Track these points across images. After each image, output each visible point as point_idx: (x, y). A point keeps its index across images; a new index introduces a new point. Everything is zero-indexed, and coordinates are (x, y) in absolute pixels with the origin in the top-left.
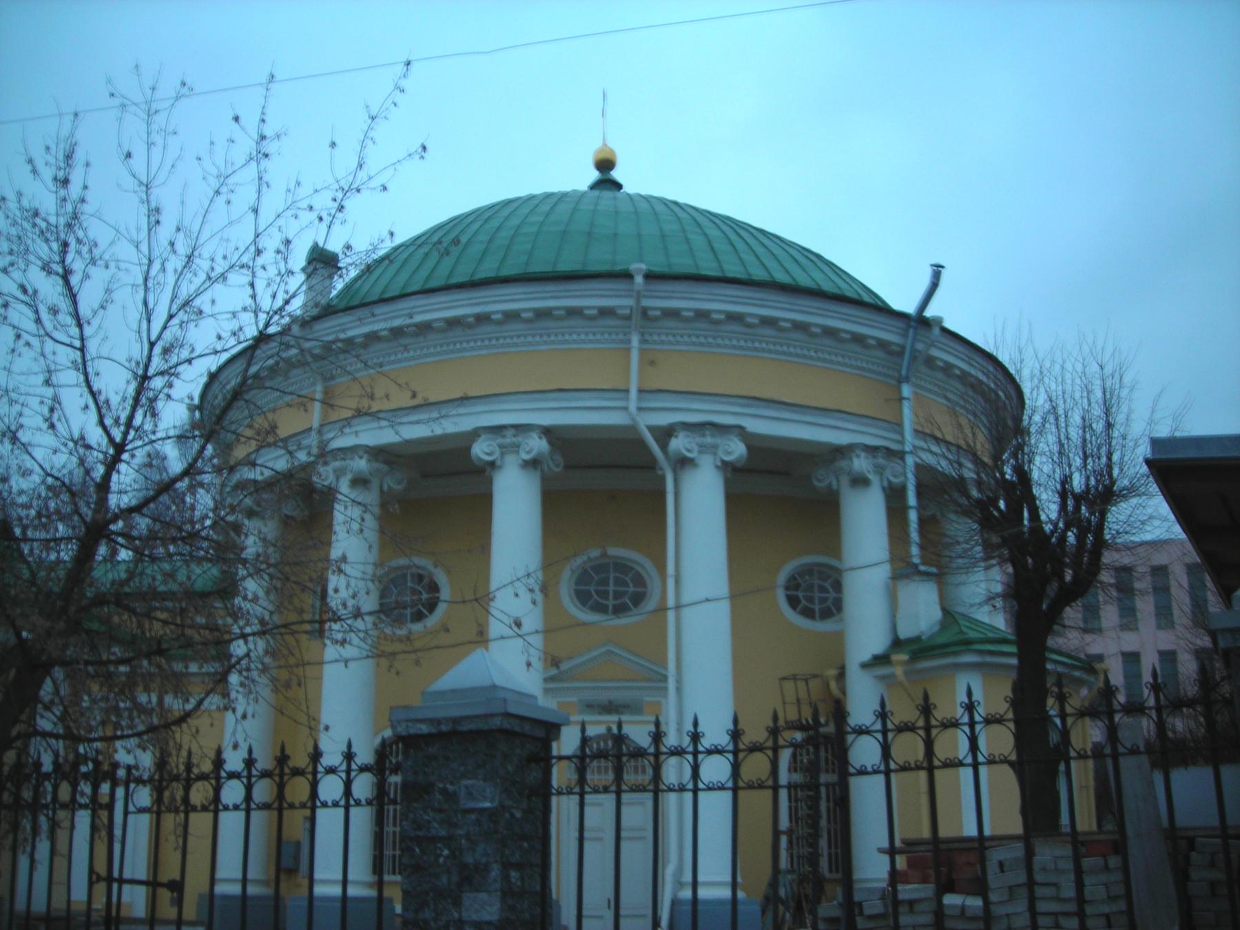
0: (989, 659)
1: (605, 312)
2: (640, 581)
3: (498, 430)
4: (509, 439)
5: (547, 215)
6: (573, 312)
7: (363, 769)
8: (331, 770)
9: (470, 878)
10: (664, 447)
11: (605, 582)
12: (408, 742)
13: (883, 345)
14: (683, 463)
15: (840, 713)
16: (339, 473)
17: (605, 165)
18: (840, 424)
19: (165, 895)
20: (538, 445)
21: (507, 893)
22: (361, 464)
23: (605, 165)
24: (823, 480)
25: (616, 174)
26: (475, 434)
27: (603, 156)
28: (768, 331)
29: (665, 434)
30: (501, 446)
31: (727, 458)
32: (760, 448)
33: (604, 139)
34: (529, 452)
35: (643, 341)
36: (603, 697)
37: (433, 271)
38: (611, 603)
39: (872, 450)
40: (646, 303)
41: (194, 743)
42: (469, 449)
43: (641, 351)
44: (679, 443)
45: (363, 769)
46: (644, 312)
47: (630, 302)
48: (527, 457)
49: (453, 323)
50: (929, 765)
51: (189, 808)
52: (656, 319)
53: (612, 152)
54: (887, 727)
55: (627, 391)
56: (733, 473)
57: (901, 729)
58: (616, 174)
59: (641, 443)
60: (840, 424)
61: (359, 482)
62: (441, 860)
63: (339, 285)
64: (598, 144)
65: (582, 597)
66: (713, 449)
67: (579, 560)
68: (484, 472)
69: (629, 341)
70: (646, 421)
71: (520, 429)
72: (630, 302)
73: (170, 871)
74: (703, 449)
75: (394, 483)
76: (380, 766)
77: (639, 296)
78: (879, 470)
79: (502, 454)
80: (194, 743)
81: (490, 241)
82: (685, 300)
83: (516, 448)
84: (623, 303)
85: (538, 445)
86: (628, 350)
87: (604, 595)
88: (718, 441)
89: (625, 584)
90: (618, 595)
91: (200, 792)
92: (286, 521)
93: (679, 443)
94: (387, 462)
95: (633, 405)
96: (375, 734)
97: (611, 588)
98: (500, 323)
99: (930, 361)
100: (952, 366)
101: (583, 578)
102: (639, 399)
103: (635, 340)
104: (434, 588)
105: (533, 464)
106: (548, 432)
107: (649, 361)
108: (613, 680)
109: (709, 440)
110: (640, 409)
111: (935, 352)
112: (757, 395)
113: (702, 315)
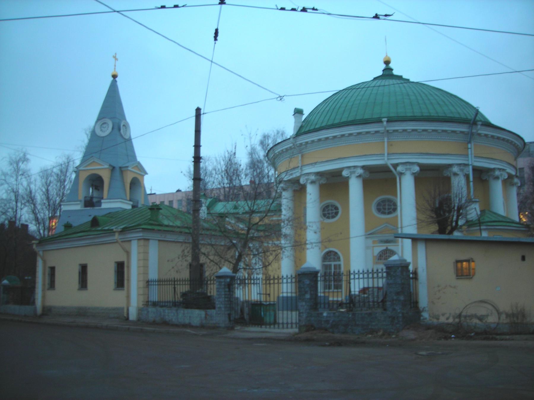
0: (489, 227)
1: (377, 132)
3: (349, 167)
4: (352, 170)
5: (363, 96)
6: (368, 133)
9: (306, 293)
10: (395, 169)
11: (385, 205)
12: (299, 275)
13: (462, 132)
14: (401, 174)
15: (350, 272)
17: (387, 62)
18: (449, 158)
19: (268, 296)
20: (360, 171)
21: (311, 294)
22: (313, 178)
23: (387, 62)
24: (446, 173)
27: (386, 60)
28: (425, 133)
29: (395, 166)
32: (424, 168)
33: (387, 54)
35: (388, 139)
36: (385, 238)
38: (387, 211)
39: (459, 165)
40: (387, 129)
41: (272, 271)
43: (388, 142)
44: (399, 169)
46: (388, 131)
47: (383, 129)
48: (358, 175)
49: (335, 137)
51: (270, 284)
52: (391, 133)
53: (389, 58)
54: (330, 281)
55: (384, 154)
60: (449, 158)
63: (304, 117)
64: (384, 56)
65: (379, 210)
66: (410, 169)
69: (384, 139)
71: (355, 167)
72: (383, 129)
73: (268, 292)
74: (407, 169)
75: (323, 181)
76: (295, 277)
77: (385, 127)
78: (462, 170)
79: (351, 174)
80: (272, 271)
81: (346, 106)
82: (399, 126)
83: (354, 172)
84: (381, 129)
85: (360, 171)
86: (384, 142)
87: (385, 209)
88: (411, 167)
90: (389, 209)
91: (272, 282)
92: (295, 191)
94: (321, 176)
95: (386, 158)
96: (322, 252)
97: (387, 207)
98: (348, 136)
99: (479, 135)
100: (488, 135)
102: (388, 156)
103: (386, 140)
105: (360, 176)
106: (363, 167)
107: (390, 145)
109: (408, 167)
110: (388, 159)
111: (479, 132)
113: (404, 131)
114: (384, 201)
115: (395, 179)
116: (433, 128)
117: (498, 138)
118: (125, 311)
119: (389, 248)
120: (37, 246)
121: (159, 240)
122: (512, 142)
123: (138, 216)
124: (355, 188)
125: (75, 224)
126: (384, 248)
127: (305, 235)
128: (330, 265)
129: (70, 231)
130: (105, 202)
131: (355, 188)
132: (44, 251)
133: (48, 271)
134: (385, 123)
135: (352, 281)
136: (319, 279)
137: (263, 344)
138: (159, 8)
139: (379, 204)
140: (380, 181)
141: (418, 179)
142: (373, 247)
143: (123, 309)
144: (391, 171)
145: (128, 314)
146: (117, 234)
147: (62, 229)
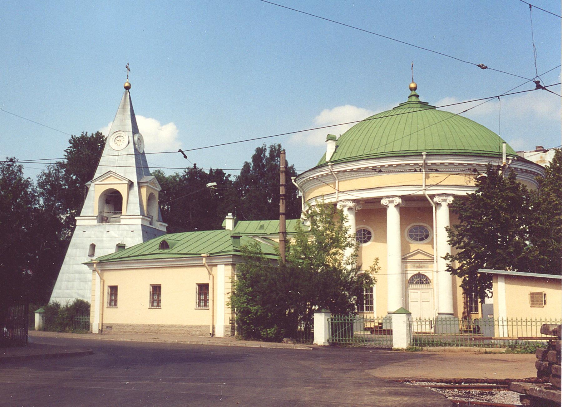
2: (427, 231)
3: (388, 197)
4: (391, 199)
14: (438, 205)
16: (344, 206)
22: (351, 204)
25: (417, 92)
29: (432, 197)
42: (380, 202)
44: (436, 199)
47: (423, 162)
50: (421, 325)
58: (417, 92)
61: (350, 209)
66: (445, 200)
67: (409, 227)
68: (383, 210)
70: (427, 193)
71: (393, 196)
75: (358, 208)
85: (398, 201)
93: (436, 199)
94: (357, 202)
101: (411, 231)
104: (369, 233)
106: (402, 197)
108: (369, 158)
109: (444, 198)
112: (457, 184)
114: (416, 228)
115: (432, 207)
116: (478, 163)
117: (527, 171)
119: (421, 272)
120: (97, 265)
121: (225, 264)
124: (393, 216)
125: (128, 245)
126: (417, 272)
129: (123, 253)
130: (79, 219)
131: (393, 216)
132: (101, 270)
133: (107, 290)
134: (424, 157)
140: (417, 211)
141: (454, 210)
144: (427, 200)
145: (213, 331)
146: (204, 259)
147: (113, 250)
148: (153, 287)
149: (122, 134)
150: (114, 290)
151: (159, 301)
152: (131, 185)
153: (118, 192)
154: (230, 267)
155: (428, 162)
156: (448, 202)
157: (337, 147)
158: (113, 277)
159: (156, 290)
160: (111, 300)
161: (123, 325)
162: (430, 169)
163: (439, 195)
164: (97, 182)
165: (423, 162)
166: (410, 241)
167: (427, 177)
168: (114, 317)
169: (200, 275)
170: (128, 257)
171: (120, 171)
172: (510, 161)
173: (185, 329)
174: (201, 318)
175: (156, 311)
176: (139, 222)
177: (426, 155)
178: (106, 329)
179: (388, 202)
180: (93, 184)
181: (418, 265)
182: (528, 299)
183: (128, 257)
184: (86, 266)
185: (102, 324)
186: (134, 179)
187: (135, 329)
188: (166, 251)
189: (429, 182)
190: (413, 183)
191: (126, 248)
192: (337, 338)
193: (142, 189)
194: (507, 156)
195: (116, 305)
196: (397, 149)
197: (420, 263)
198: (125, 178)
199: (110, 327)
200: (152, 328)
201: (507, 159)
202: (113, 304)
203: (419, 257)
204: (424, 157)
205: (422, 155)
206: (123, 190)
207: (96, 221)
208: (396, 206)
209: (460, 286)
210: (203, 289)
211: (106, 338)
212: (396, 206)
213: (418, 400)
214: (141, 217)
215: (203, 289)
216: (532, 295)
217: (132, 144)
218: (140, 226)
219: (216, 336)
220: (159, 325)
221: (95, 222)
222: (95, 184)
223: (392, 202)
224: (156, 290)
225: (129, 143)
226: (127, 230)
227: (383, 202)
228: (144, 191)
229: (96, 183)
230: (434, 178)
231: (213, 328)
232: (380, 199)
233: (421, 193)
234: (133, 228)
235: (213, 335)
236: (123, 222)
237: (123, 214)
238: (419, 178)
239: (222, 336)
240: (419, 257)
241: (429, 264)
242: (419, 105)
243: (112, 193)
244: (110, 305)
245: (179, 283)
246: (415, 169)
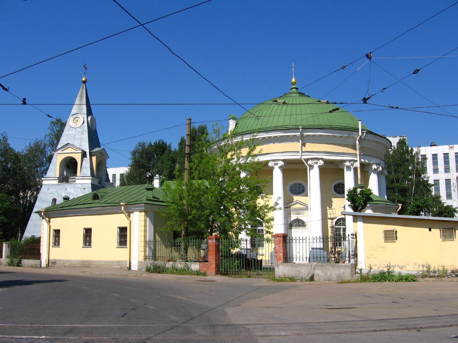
2: (303, 187)
3: (274, 160)
4: (276, 162)
7: (321, 239)
8: (304, 239)
10: (307, 162)
14: (311, 167)
26: (269, 161)
29: (307, 160)
30: (274, 163)
31: (320, 165)
32: (326, 162)
34: (280, 165)
37: (398, 330)
44: (310, 162)
45: (321, 239)
56: (321, 168)
57: (314, 239)
59: (302, 161)
62: (428, 187)
66: (316, 163)
71: (278, 160)
79: (275, 165)
85: (281, 163)
89: (300, 188)
93: (310, 162)
100: (370, 140)
109: (316, 161)
114: (295, 185)
117: (377, 142)
118: (128, 263)
119: (299, 218)
122: (382, 143)
123: (119, 193)
124: (278, 176)
125: (71, 198)
127: (370, 209)
128: (340, 228)
131: (278, 176)
134: (301, 130)
135: (157, 246)
136: (329, 240)
137: (179, 297)
138: (333, 103)
139: (291, 187)
142: (288, 217)
143: (126, 262)
144: (304, 163)
145: (130, 266)
148: (85, 230)
149: (79, 115)
150: (57, 232)
151: (90, 242)
152: (84, 155)
153: (74, 159)
154: (143, 213)
155: (304, 134)
156: (319, 164)
157: (236, 124)
158: (57, 223)
159: (88, 232)
160: (55, 242)
161: (64, 261)
162: (304, 140)
163: (312, 159)
164: (59, 152)
165: (299, 134)
166: (292, 195)
167: (303, 145)
168: (58, 254)
169: (119, 220)
170: (69, 206)
171: (76, 143)
172: (365, 134)
173: (109, 263)
174: (121, 255)
175: (88, 249)
176: (90, 181)
177: (302, 129)
178: (50, 263)
179: (274, 164)
180: (56, 153)
181: (297, 212)
182: (382, 236)
183: (69, 206)
184: (35, 213)
185: (49, 259)
186: (87, 151)
187: (72, 265)
188: (97, 201)
189: (304, 149)
190: (292, 150)
191: (70, 199)
192: (234, 270)
193: (93, 157)
194: (362, 130)
195: (59, 244)
196: (280, 124)
197: (298, 211)
198: (80, 149)
199: (54, 262)
200: (85, 263)
201: (362, 132)
202: (57, 244)
203: (298, 206)
204: (301, 130)
205: (299, 129)
206: (78, 157)
207: (57, 181)
208: (279, 167)
209: (298, 218)
210: (123, 232)
211: (52, 271)
212: (279, 167)
213: (116, 342)
214: (91, 178)
215: (123, 232)
216: (386, 232)
217: (86, 123)
218: (90, 184)
219: (132, 270)
220: (67, 260)
221: (56, 182)
222: (57, 153)
223: (277, 164)
224: (88, 232)
225: (84, 122)
226: (80, 188)
227: (270, 164)
228: (94, 158)
229: (58, 152)
230: (309, 146)
231: (130, 263)
232: (267, 162)
233: (298, 157)
234: (85, 186)
235: (130, 268)
236: (77, 181)
237: (78, 176)
238: (297, 146)
239: (137, 269)
240: (298, 206)
241: (305, 212)
242: (298, 95)
243: (70, 160)
244: (55, 245)
245: (105, 226)
246: (293, 139)
